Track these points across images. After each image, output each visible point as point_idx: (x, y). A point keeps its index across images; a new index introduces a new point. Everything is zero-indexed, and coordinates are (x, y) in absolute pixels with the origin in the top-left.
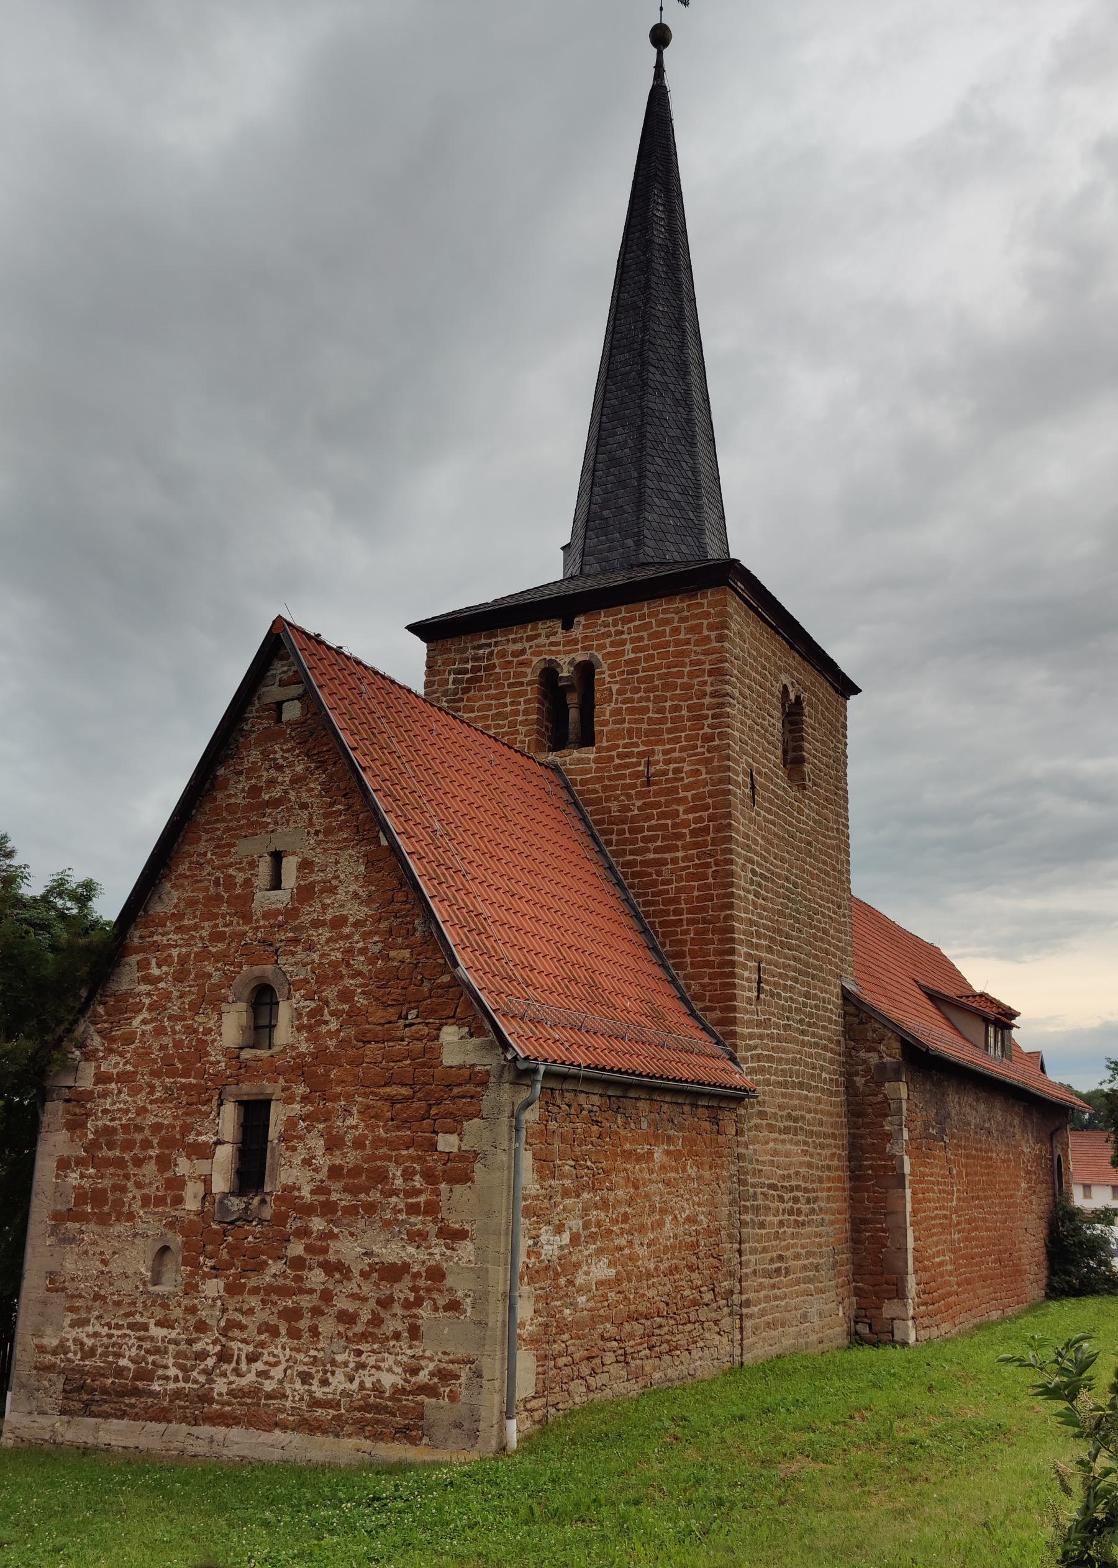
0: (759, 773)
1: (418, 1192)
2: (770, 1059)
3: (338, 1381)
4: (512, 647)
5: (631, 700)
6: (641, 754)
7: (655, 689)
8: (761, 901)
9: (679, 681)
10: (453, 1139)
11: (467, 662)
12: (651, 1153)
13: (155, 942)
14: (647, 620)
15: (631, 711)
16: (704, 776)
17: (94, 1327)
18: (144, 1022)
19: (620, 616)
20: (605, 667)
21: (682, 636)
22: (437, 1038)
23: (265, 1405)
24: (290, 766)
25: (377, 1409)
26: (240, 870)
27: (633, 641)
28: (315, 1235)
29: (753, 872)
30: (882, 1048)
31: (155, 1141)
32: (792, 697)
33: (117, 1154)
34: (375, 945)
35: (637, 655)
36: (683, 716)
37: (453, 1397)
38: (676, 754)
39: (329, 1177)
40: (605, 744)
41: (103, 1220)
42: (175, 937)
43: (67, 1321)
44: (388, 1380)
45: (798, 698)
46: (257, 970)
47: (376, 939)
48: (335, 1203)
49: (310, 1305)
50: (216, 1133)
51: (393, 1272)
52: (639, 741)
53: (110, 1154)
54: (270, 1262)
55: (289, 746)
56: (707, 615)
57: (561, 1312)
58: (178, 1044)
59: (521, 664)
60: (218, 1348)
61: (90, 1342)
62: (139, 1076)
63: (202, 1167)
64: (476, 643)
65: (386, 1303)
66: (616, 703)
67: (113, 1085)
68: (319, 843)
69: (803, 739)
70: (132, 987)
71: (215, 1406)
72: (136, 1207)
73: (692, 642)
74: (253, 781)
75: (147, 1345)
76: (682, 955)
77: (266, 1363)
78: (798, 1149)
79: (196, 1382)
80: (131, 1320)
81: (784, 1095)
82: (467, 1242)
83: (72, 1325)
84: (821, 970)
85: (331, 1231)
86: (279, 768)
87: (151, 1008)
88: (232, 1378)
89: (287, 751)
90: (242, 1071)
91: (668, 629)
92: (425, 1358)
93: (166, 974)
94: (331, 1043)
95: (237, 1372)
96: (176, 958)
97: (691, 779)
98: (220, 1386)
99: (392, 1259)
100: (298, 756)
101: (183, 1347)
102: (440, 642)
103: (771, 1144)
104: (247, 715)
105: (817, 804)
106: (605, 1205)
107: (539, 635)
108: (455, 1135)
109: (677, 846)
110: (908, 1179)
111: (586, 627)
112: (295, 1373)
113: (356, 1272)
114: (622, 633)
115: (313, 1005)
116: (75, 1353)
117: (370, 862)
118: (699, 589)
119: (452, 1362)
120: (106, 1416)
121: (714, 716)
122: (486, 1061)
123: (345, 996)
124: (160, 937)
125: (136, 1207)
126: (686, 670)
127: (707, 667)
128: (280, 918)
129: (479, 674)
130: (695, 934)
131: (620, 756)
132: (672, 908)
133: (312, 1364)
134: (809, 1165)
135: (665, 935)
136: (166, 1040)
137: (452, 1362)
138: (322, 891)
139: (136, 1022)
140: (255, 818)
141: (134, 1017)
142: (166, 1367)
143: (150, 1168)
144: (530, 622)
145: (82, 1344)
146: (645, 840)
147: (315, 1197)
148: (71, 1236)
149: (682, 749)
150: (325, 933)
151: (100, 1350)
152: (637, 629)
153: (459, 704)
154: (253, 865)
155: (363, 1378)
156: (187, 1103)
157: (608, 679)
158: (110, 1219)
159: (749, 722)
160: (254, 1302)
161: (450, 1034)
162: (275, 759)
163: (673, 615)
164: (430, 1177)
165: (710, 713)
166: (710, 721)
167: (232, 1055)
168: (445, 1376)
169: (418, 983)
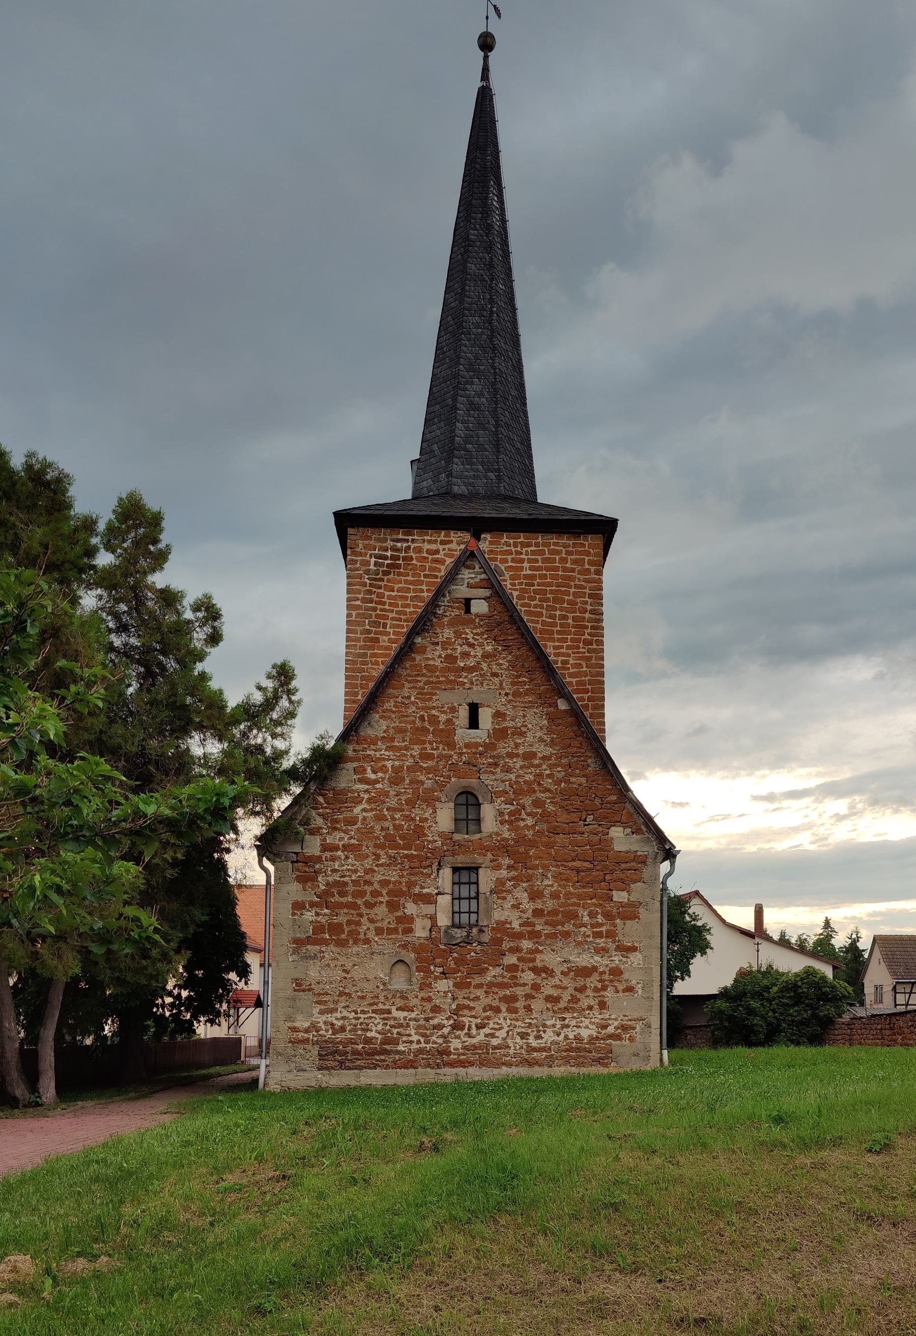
1: (602, 925)
3: (549, 1036)
4: (426, 546)
5: (529, 606)
7: (548, 600)
9: (566, 598)
11: (386, 550)
14: (541, 548)
16: (585, 669)
18: (364, 810)
19: (519, 540)
20: (507, 577)
21: (568, 565)
23: (492, 1053)
25: (578, 1049)
26: (442, 712)
27: (529, 561)
28: (525, 951)
31: (384, 892)
33: (350, 900)
34: (559, 773)
35: (533, 572)
36: (569, 624)
37: (632, 1039)
38: (564, 650)
39: (533, 916)
41: (341, 944)
42: (387, 753)
44: (585, 1033)
46: (465, 782)
47: (559, 769)
48: (539, 932)
49: (523, 993)
50: (437, 888)
54: (491, 968)
55: (478, 631)
56: (588, 554)
58: (397, 828)
59: (436, 561)
60: (452, 1022)
61: (339, 1023)
62: (364, 848)
63: (429, 909)
64: (394, 537)
65: (581, 990)
67: (339, 853)
70: (350, 785)
72: (371, 935)
73: (576, 571)
74: (449, 652)
77: (492, 1029)
79: (436, 1043)
80: (375, 1007)
83: (322, 1013)
86: (472, 646)
88: (465, 1039)
89: (477, 634)
90: (457, 847)
91: (557, 557)
93: (383, 779)
95: (469, 1035)
96: (390, 768)
97: (575, 670)
99: (584, 964)
100: (486, 639)
101: (422, 1022)
102: (361, 529)
104: (440, 603)
107: (451, 542)
112: (515, 1034)
113: (558, 972)
114: (521, 553)
115: (512, 808)
116: (327, 1031)
117: (551, 718)
119: (630, 1020)
120: (360, 1068)
121: (592, 628)
123: (538, 803)
124: (373, 752)
125: (371, 935)
126: (572, 590)
127: (587, 591)
129: (397, 562)
133: (529, 1027)
136: (386, 824)
137: (630, 1020)
138: (513, 734)
139: (357, 810)
140: (453, 678)
141: (355, 807)
142: (409, 1035)
144: (443, 529)
145: (332, 1025)
147: (523, 928)
148: (313, 955)
149: (568, 647)
151: (348, 1028)
152: (533, 553)
153: (380, 583)
154: (453, 710)
156: (410, 867)
158: (348, 943)
160: (479, 993)
161: (616, 832)
162: (467, 639)
163: (562, 548)
164: (608, 916)
165: (589, 625)
166: (589, 631)
167: (446, 837)
168: (626, 1028)
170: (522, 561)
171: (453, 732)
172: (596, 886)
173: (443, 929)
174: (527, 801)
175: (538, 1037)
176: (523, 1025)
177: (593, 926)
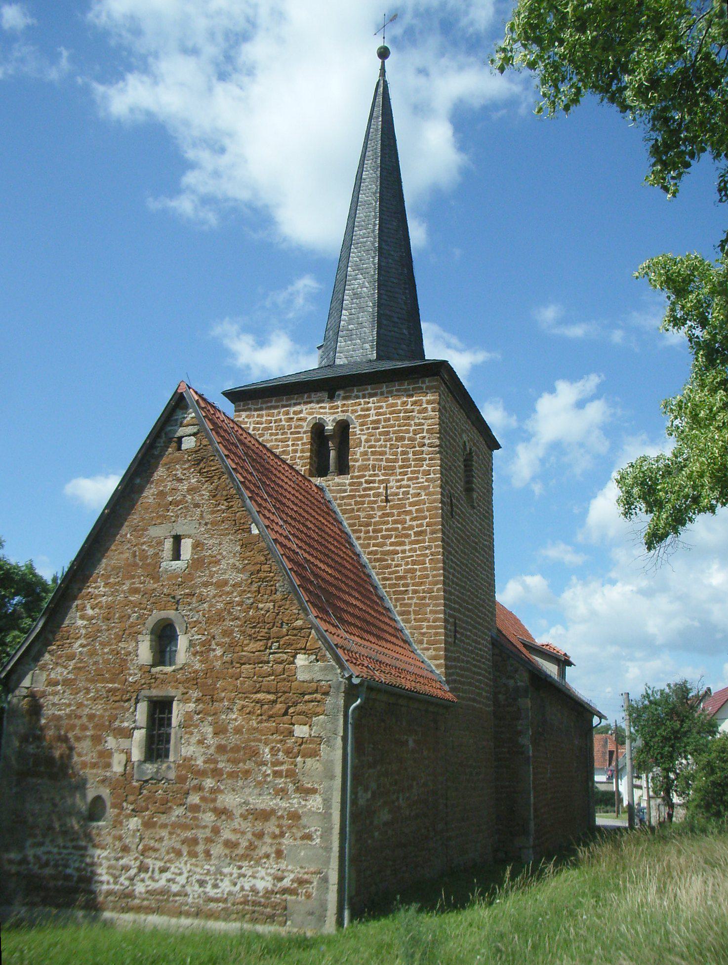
0: (454, 497)
1: (282, 763)
3: (226, 886)
5: (374, 446)
6: (381, 482)
7: (390, 439)
8: (455, 579)
10: (306, 728)
13: (90, 592)
15: (373, 453)
22: (293, 663)
25: (255, 903)
32: (468, 449)
38: (405, 482)
40: (357, 474)
44: (261, 885)
45: (470, 449)
46: (163, 614)
47: (249, 595)
48: (221, 769)
49: (204, 836)
51: (265, 815)
52: (380, 473)
55: (186, 466)
59: (300, 419)
61: (45, 858)
63: (124, 743)
65: (260, 835)
66: (364, 447)
67: (59, 687)
68: (207, 531)
69: (473, 476)
74: (161, 488)
76: (409, 613)
77: (173, 873)
79: (122, 885)
80: (74, 843)
82: (317, 796)
87: (87, 636)
94: (218, 664)
95: (152, 878)
97: (414, 499)
98: (140, 888)
99: (262, 806)
105: (480, 518)
108: (307, 727)
111: (345, 398)
113: (237, 812)
114: (369, 403)
122: (328, 678)
124: (93, 589)
126: (412, 429)
127: (426, 427)
128: (180, 579)
131: (366, 482)
135: (397, 600)
146: (383, 537)
147: (207, 765)
149: (409, 479)
150: (212, 591)
154: (160, 543)
155: (243, 883)
157: (358, 432)
159: (449, 464)
160: (164, 833)
165: (427, 457)
166: (427, 462)
167: (146, 670)
169: (280, 625)
170: (368, 409)
171: (157, 565)
172: (279, 719)
173: (136, 764)
174: (216, 630)
175: (215, 886)
176: (201, 872)
177: (274, 764)
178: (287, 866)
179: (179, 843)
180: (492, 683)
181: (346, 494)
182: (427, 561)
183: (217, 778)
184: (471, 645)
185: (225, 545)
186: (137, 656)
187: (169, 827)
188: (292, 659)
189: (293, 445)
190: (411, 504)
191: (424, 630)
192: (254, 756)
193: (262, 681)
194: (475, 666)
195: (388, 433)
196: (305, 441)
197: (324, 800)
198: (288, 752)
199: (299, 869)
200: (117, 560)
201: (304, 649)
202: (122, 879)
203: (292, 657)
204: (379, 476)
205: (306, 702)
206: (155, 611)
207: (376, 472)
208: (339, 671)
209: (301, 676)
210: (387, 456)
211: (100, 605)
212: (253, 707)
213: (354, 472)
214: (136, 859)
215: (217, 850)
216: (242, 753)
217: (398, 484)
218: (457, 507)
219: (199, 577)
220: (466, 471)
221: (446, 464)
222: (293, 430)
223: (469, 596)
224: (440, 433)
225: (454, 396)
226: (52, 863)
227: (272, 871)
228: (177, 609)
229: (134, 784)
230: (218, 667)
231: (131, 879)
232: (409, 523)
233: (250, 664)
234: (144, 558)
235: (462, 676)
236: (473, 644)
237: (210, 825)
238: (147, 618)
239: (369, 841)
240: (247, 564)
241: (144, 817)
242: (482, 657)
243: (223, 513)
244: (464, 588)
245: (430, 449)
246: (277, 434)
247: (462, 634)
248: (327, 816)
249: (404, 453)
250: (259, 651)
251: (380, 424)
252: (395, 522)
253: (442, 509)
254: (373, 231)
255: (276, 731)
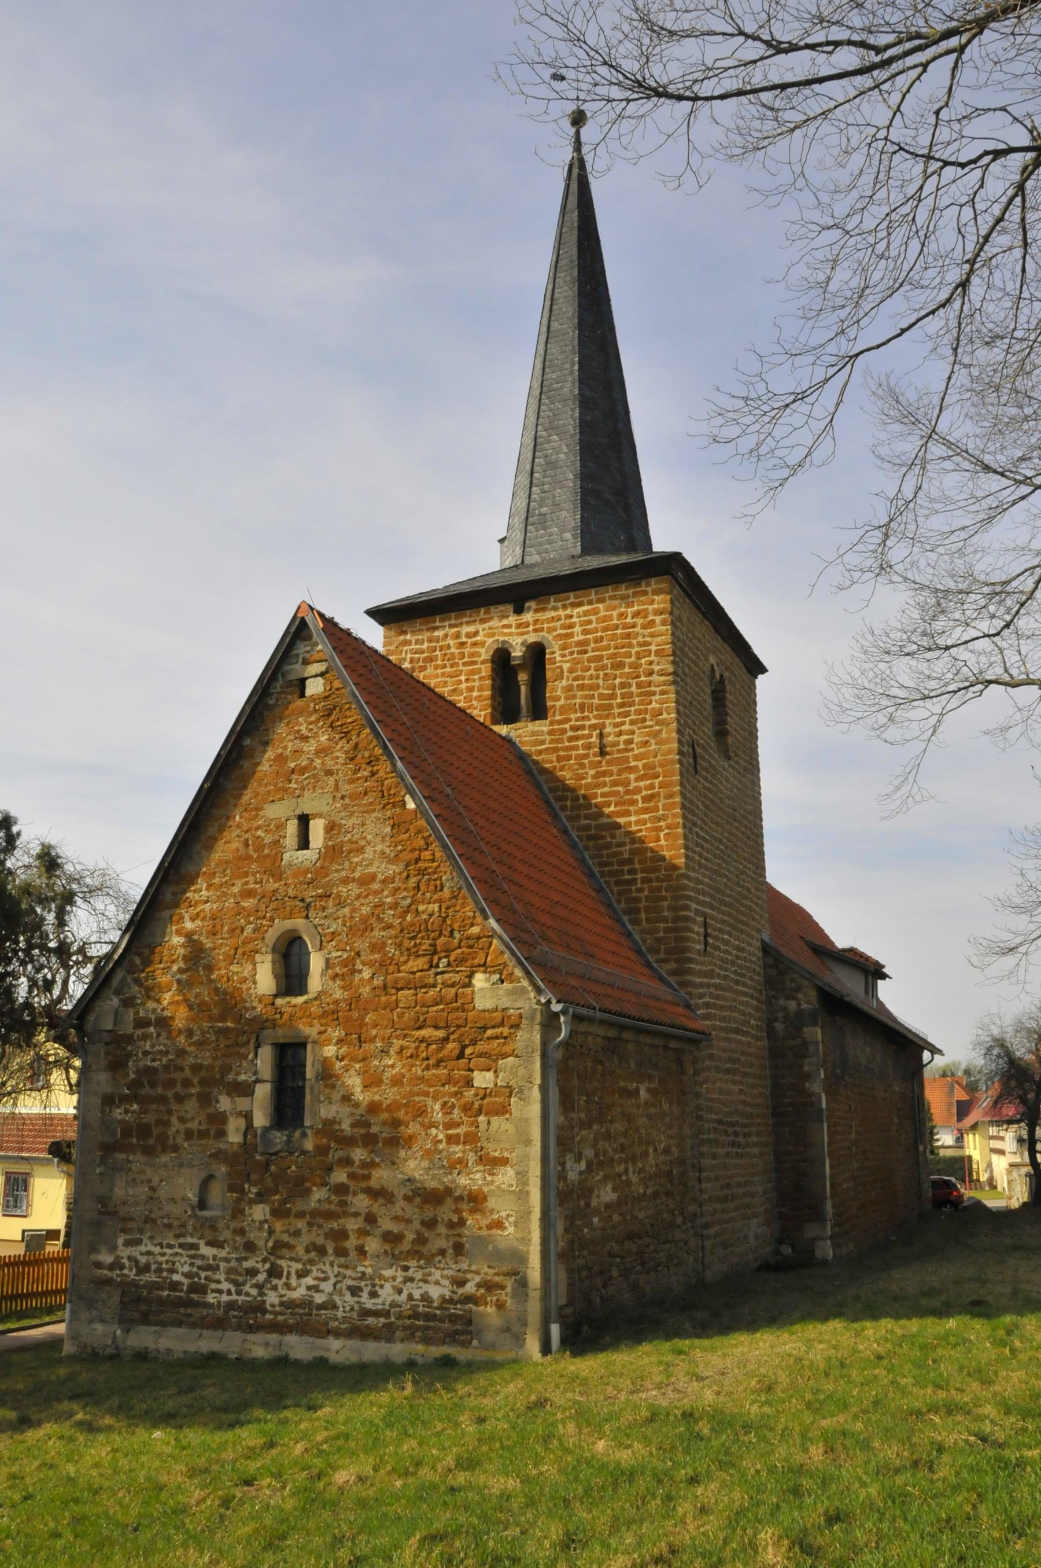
0: (698, 744)
1: (458, 1125)
2: (715, 1006)
3: (387, 1294)
6: (593, 727)
8: (703, 861)
10: (490, 1075)
12: (637, 1090)
15: (581, 687)
17: (148, 1246)
20: (556, 648)
22: (469, 985)
24: (315, 737)
25: (428, 1317)
29: (698, 835)
30: (800, 996)
31: (196, 1081)
32: (718, 675)
38: (626, 727)
40: (558, 718)
41: (148, 1151)
43: (120, 1241)
44: (435, 1292)
45: (721, 676)
46: (288, 924)
47: (404, 894)
49: (356, 1227)
52: (591, 715)
53: (152, 1092)
55: (313, 718)
57: (582, 1230)
59: (475, 644)
61: (143, 1260)
63: (242, 1103)
65: (430, 1224)
67: (152, 1029)
68: (345, 807)
69: (726, 714)
71: (268, 1316)
72: (179, 1140)
74: (280, 751)
75: (199, 1262)
77: (316, 1278)
78: (736, 1088)
79: (247, 1294)
80: (182, 1240)
81: (726, 1039)
84: (748, 925)
85: (373, 1160)
88: (283, 1292)
90: (278, 1016)
92: (471, 1272)
94: (366, 991)
103: (718, 1084)
104: (272, 691)
105: (739, 773)
106: (608, 1136)
109: (630, 811)
110: (825, 1113)
111: (537, 611)
113: (399, 1193)
114: (571, 617)
116: (131, 1270)
118: (644, 578)
120: (164, 1324)
122: (518, 1005)
126: (633, 651)
127: (653, 648)
128: (309, 875)
130: (650, 891)
131: (573, 729)
132: (626, 868)
134: (744, 1103)
142: (218, 1282)
143: (191, 1106)
144: (482, 606)
145: (137, 1262)
147: (356, 1130)
149: (632, 723)
152: (586, 613)
154: (281, 826)
160: (301, 1224)
165: (658, 689)
176: (354, 1275)
177: (448, 1126)
178: (469, 1266)
179: (322, 1237)
180: (764, 1007)
181: (543, 747)
182: (662, 837)
183: (370, 1147)
184: (731, 954)
185: (370, 826)
186: (255, 983)
187: (308, 1216)
188: (467, 980)
189: (467, 680)
190: (637, 758)
191: (661, 934)
192: (420, 1116)
193: (428, 1012)
194: (737, 982)
195: (599, 658)
196: (483, 674)
197: (518, 1173)
198: (466, 1109)
199: (486, 1269)
200: (223, 851)
201: (484, 965)
202: (247, 1288)
203: (467, 977)
204: (590, 720)
205: (488, 1038)
206: (277, 921)
207: (586, 714)
208: (532, 995)
209: (482, 1003)
210: (601, 691)
211: (202, 915)
212: (417, 1048)
213: (554, 715)
214: (264, 1261)
215: (373, 1245)
216: (403, 1112)
217: (617, 729)
218: (703, 758)
219: (337, 871)
220: (715, 707)
221: (685, 699)
222: (466, 660)
223: (726, 885)
224: (674, 654)
225: (693, 601)
226: (153, 1267)
227: (449, 1273)
228: (307, 917)
229: (258, 1157)
230: (365, 995)
231: (259, 1287)
232: (633, 785)
233: (410, 989)
234: (259, 848)
235: (717, 997)
236: (734, 952)
237: (364, 1212)
238: (267, 931)
239: (586, 1230)
240: (401, 851)
241: (273, 1203)
242: (748, 969)
243: (366, 781)
244: (716, 872)
245: (662, 678)
246: (445, 666)
247: (716, 938)
248: (522, 1195)
249: (623, 685)
250: (422, 971)
251: (588, 645)
252: (615, 783)
253: (680, 762)
254: (571, 373)
255: (449, 1081)
